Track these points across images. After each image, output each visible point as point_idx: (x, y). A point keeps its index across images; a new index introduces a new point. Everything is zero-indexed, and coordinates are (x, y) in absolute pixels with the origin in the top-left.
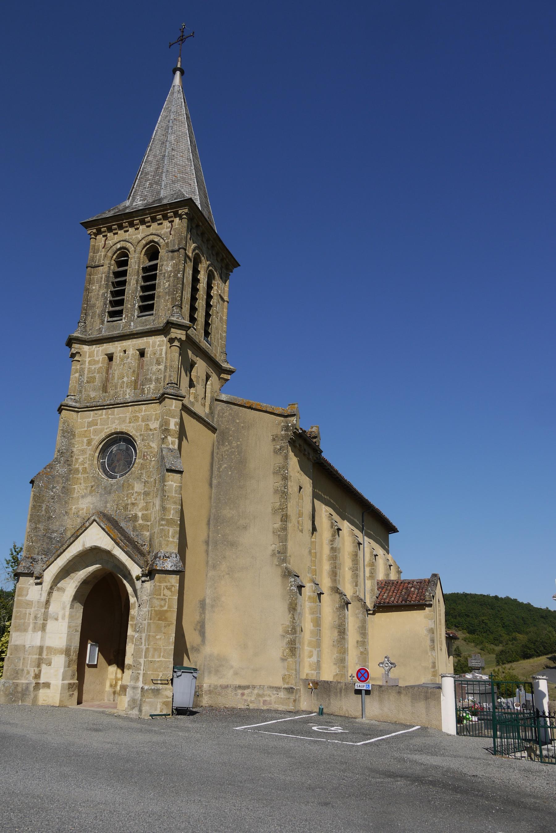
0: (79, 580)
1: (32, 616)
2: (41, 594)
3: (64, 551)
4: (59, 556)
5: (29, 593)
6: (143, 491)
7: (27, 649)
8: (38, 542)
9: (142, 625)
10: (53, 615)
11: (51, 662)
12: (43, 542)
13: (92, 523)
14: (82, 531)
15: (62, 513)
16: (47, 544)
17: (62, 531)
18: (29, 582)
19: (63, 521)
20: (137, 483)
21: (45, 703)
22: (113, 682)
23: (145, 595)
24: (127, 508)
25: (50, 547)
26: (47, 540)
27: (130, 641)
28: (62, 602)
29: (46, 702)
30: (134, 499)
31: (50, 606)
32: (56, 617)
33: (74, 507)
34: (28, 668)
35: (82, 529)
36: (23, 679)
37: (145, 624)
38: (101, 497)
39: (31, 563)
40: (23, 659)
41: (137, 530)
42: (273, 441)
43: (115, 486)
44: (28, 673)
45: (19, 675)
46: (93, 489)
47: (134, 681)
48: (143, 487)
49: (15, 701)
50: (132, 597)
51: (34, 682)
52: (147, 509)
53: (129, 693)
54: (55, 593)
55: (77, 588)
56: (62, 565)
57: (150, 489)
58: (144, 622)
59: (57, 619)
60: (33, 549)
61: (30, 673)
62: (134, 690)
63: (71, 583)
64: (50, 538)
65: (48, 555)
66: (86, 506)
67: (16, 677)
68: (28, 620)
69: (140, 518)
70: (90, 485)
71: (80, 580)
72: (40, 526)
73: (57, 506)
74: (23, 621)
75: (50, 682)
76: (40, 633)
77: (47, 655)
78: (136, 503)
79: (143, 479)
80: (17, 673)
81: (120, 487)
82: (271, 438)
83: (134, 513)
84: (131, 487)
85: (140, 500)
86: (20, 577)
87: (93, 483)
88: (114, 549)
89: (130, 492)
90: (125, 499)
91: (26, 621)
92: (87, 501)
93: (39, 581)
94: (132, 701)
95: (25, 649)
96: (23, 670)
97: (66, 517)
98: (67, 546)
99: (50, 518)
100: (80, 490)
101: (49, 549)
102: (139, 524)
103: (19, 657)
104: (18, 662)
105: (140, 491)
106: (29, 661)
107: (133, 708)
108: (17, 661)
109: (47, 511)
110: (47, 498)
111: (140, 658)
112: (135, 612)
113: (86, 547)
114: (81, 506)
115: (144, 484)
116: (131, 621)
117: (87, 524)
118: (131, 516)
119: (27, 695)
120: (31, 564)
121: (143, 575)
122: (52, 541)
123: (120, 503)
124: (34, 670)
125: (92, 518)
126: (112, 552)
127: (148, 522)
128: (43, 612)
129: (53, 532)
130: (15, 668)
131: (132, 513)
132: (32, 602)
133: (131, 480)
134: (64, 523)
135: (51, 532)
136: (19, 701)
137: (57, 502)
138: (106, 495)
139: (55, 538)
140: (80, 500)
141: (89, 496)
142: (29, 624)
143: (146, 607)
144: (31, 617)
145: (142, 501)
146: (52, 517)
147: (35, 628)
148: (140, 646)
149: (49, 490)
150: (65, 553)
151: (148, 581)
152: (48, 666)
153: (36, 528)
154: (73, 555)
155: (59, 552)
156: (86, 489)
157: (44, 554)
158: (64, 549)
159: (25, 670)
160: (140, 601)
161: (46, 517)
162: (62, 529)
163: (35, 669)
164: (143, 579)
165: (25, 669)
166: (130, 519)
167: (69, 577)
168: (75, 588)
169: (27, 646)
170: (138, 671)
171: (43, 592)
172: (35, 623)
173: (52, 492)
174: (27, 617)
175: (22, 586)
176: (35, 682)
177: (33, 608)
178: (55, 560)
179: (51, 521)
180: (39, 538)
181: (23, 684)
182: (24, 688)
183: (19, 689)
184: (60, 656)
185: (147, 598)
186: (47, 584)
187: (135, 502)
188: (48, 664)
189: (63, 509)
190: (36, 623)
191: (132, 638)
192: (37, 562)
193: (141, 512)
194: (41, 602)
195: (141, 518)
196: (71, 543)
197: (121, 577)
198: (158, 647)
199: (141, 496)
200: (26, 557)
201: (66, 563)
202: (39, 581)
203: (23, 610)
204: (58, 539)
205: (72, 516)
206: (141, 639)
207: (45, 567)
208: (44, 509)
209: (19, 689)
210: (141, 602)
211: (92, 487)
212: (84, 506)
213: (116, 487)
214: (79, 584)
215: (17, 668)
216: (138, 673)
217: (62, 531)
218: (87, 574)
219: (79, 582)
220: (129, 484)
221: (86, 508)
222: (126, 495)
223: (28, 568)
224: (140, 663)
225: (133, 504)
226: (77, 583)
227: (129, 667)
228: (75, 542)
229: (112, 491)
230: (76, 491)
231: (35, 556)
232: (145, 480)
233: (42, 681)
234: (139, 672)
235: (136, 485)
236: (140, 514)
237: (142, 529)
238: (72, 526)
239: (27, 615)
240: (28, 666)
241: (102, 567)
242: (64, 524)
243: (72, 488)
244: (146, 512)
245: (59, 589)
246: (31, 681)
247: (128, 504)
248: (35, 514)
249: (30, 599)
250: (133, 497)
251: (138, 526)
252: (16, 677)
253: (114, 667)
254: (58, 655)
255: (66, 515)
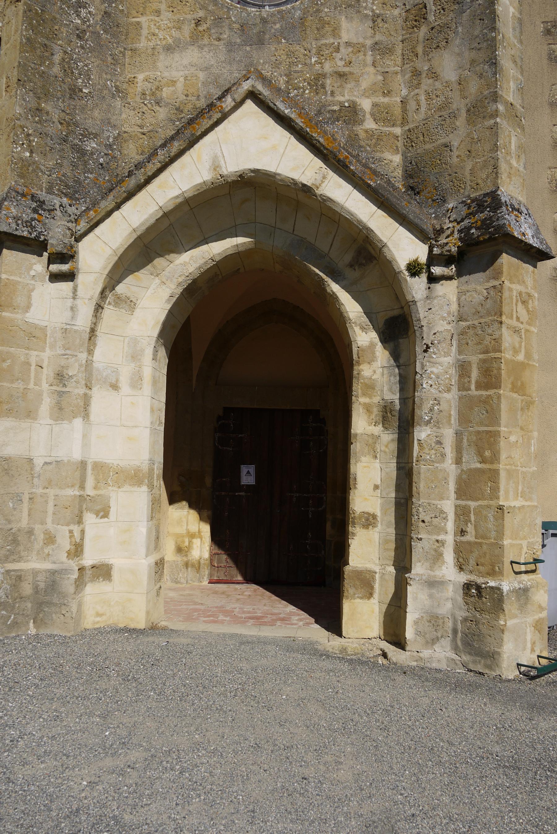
0: (180, 280)
1: (48, 373)
2: (72, 308)
3: (148, 181)
4: (130, 195)
5: (33, 301)
6: (369, 42)
7: (37, 469)
8: (49, 155)
9: (439, 404)
10: (105, 374)
11: (109, 507)
12: (62, 157)
13: (241, 103)
14: (211, 122)
15: (106, 85)
16: (74, 166)
17: (111, 140)
18: (31, 268)
19: (112, 111)
20: (349, 19)
21: (101, 622)
22: (183, 542)
23: (444, 319)
24: (323, 86)
25: (82, 178)
26: (73, 156)
27: (366, 450)
28: (127, 340)
29: (104, 618)
30: (343, 63)
31: (97, 348)
32: (114, 381)
33: (141, 77)
34: (50, 526)
35: (210, 118)
36: (35, 558)
37: (448, 401)
38: (230, 51)
39: (35, 211)
40: (30, 499)
41: (361, 147)
42: (546, 35)
43: (275, 23)
44: (50, 539)
45: (21, 548)
46: (201, 28)
47: (427, 564)
48: (370, 31)
49: (15, 624)
50: (363, 329)
51: (74, 565)
52: (389, 92)
53: (415, 599)
54: (109, 312)
55: (172, 303)
56: (142, 224)
57: (392, 38)
58: (446, 395)
59: (115, 387)
60: (34, 171)
61: (59, 540)
62: (434, 591)
63: (153, 286)
64: (82, 152)
65: (78, 199)
66: (182, 73)
67: (11, 552)
68: (36, 384)
69: (368, 116)
70: (189, 17)
71: (183, 278)
72: (49, 108)
73: (93, 63)
74: (20, 385)
75: (111, 562)
76: (78, 422)
77: (95, 488)
78: (351, 73)
79: (365, 8)
80: (15, 541)
81: (294, 27)
82: (541, 28)
83: (348, 101)
84: (327, 28)
85: (365, 65)
86: (5, 251)
87: (201, 14)
88: (326, 182)
89: (327, 42)
90: (313, 60)
91: (31, 386)
92: (185, 62)
93: (65, 268)
94: (430, 621)
95: (32, 469)
96: (30, 532)
97: (118, 103)
98: (159, 165)
99: (74, 91)
100: (157, 31)
101: (78, 182)
102: (366, 131)
103: (18, 495)
104: (15, 509)
105: (361, 40)
106: (51, 504)
107: (434, 641)
108: (11, 505)
109: (67, 70)
110: (64, 30)
111: (442, 498)
112: (375, 372)
113: (225, 172)
114: (166, 74)
115: (370, 24)
116: (364, 395)
117: (229, 102)
118: (336, 108)
119: (55, 605)
120: (36, 216)
121: (432, 260)
122: (86, 163)
123: (296, 72)
124: (71, 532)
125: (246, 86)
126: (318, 192)
127: (393, 126)
128: (84, 362)
129: (87, 135)
130: (10, 526)
131: (341, 99)
132: (44, 329)
133: (326, 10)
134: (115, 117)
135: (82, 135)
136: (28, 623)
137: (92, 50)
138: (248, 48)
139: (92, 154)
140: (162, 57)
141: (192, 47)
142: (40, 395)
143: (447, 354)
144: (44, 377)
145: (371, 70)
146: (81, 90)
147: (61, 409)
148: (436, 465)
149: (68, 7)
150: (150, 188)
151: (450, 278)
152: (101, 518)
153: (37, 109)
154: (177, 197)
155: (132, 183)
156: (180, 28)
157: (66, 195)
158: (150, 174)
159: (36, 532)
160: (428, 335)
161: (66, 87)
162: (110, 134)
163: (72, 527)
164: (437, 270)
165: (38, 529)
166: (335, 117)
167: (149, 267)
168: (168, 301)
169: (39, 462)
170: (438, 534)
171: (78, 302)
172: (61, 394)
173: (78, 16)
174: (32, 375)
175: (12, 278)
176: (77, 568)
177: (47, 349)
178: (118, 207)
179: (79, 103)
180: (50, 142)
181: (35, 573)
182: (42, 585)
183: (27, 589)
184: (136, 489)
185: (449, 327)
186: (91, 278)
187: (346, 69)
188: (102, 514)
189: (109, 77)
190: (64, 392)
191: (371, 441)
192: (52, 213)
193: (368, 97)
194: (76, 331)
195: (372, 115)
196: (173, 160)
197: (321, 274)
198: (513, 467)
199: (365, 55)
200: (18, 193)
201: (153, 221)
202: (65, 268)
203: (20, 353)
204: (101, 160)
205: (138, 99)
206: (439, 443)
207: (83, 226)
208: (57, 58)
209: (27, 589)
210: (432, 337)
211: (198, 23)
212: (178, 75)
213: (278, 26)
214: (180, 290)
215: (15, 526)
216: (437, 541)
217: (111, 140)
218: (206, 263)
219: (179, 284)
220: (321, 19)
221: (182, 79)
222: (314, 51)
223: (29, 224)
224: (442, 512)
225: (341, 75)
226: (173, 287)
227: (367, 520)
228: (185, 158)
229: (267, 36)
230: (145, 32)
231: (43, 195)
232: (373, 11)
233: (88, 560)
234: (440, 538)
235: (344, 24)
236: (366, 104)
237: (376, 145)
238: (141, 127)
239: (33, 368)
240: (49, 520)
241: (253, 246)
242: (113, 119)
243: (131, 24)
244: (386, 100)
245: (119, 301)
246: (62, 563)
247: (324, 76)
248: (33, 65)
249: (36, 322)
250: (339, 56)
251: (362, 135)
252: (11, 552)
253: (182, 508)
254: (127, 488)
255: (119, 97)
